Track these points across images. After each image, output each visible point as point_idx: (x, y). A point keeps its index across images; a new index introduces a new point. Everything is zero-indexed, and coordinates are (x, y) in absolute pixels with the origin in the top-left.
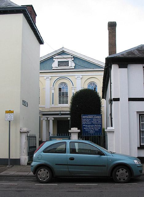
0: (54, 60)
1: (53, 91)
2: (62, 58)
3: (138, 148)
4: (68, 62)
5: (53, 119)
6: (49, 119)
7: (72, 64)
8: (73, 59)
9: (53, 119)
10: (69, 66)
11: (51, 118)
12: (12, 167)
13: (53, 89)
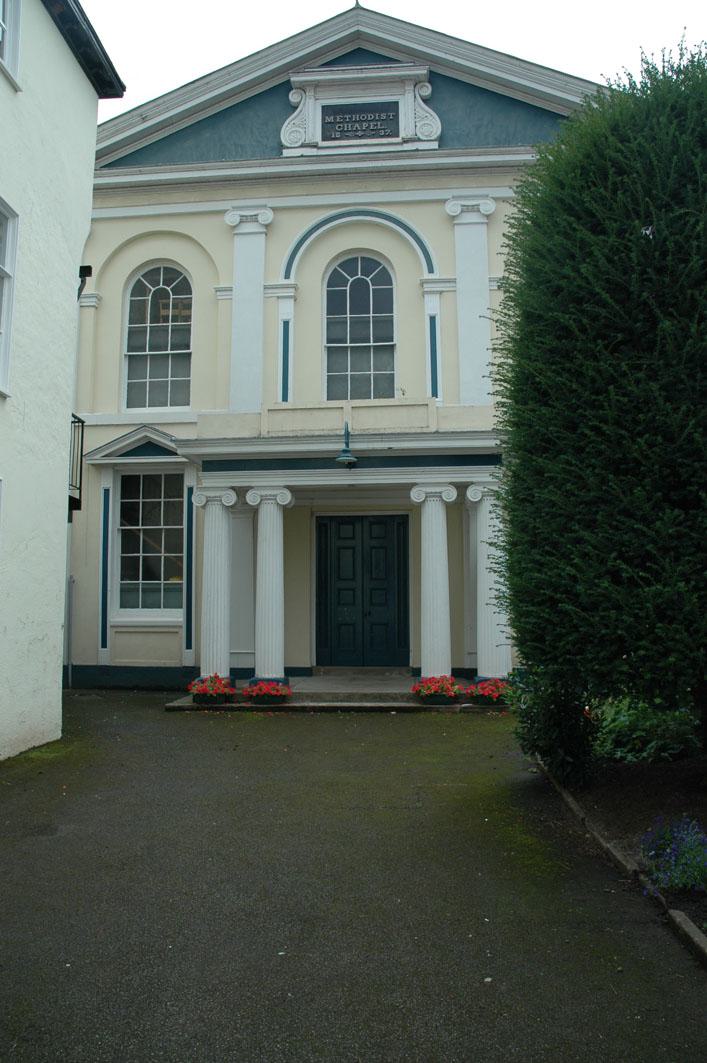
0: (293, 97)
1: (286, 310)
2: (359, 88)
3: (94, 189)
4: (394, 107)
5: (286, 498)
6: (251, 498)
7: (418, 121)
8: (427, 91)
9: (286, 498)
10: (403, 134)
11: (272, 491)
12: (478, 713)
13: (291, 292)
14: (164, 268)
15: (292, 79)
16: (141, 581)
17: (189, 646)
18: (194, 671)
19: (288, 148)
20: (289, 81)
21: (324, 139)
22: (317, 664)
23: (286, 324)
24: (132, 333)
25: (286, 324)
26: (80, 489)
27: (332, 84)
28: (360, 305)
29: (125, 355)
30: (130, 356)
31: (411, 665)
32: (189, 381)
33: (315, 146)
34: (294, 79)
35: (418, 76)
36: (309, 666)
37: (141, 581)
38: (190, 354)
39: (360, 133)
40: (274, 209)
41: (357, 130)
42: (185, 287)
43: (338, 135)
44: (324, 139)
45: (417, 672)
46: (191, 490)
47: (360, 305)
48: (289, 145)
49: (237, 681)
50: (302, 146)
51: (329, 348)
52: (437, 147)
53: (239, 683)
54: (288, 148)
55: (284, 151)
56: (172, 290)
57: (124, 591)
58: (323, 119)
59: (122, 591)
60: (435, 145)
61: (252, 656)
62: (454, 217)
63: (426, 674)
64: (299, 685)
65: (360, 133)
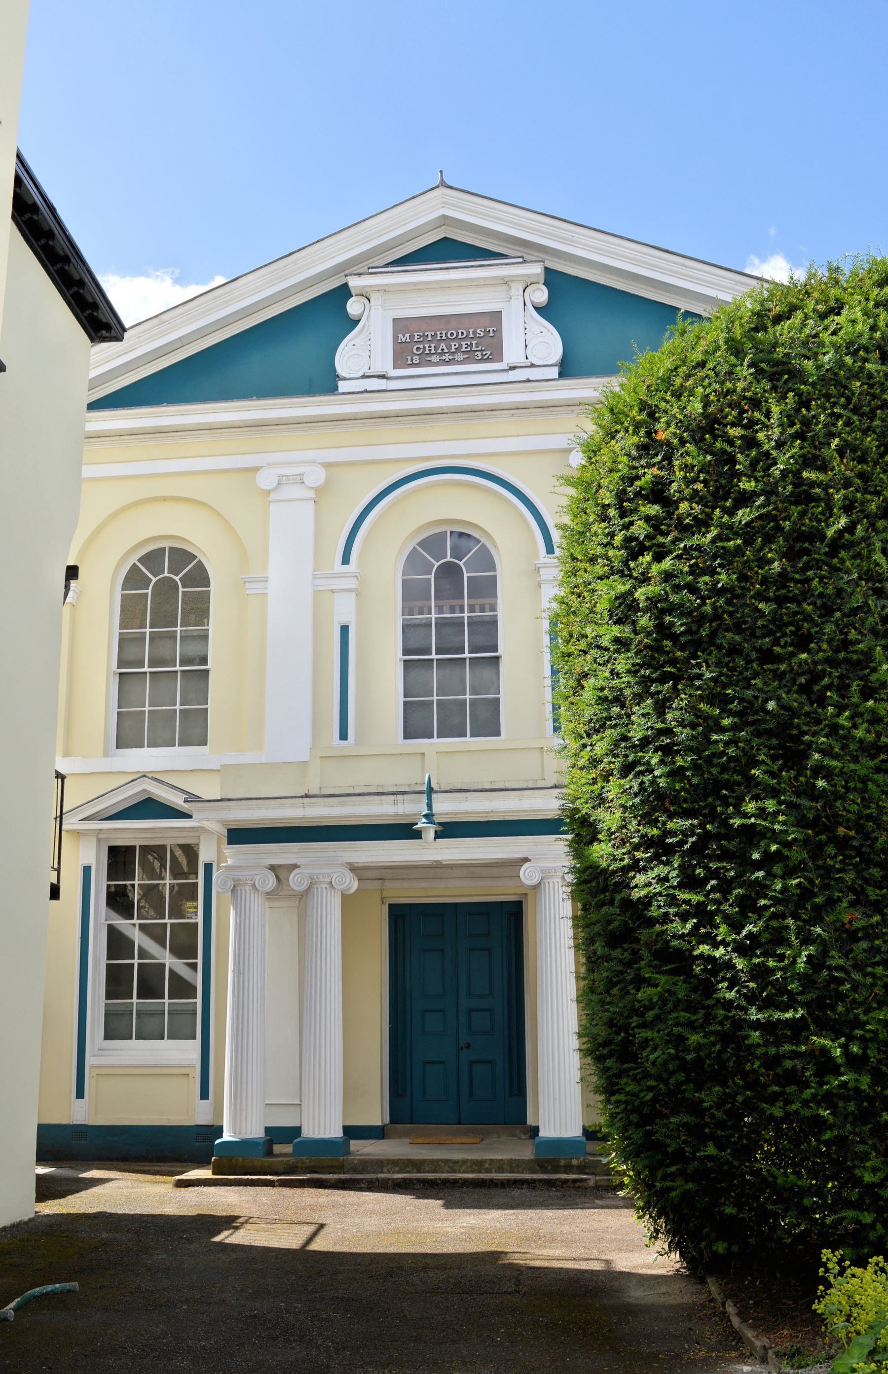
0: (353, 307)
8: (541, 295)
14: (170, 548)
15: (351, 284)
16: (135, 1000)
17: (204, 1095)
18: (297, 1131)
19: (345, 379)
20: (346, 285)
21: (395, 367)
22: (392, 1121)
23: (345, 629)
24: (123, 641)
25: (345, 629)
26: (58, 870)
27: (401, 289)
28: (164, 617)
29: (115, 673)
30: (120, 674)
31: (528, 1123)
32: (206, 710)
33: (383, 377)
34: (354, 283)
35: (528, 276)
36: (379, 1123)
37: (135, 1000)
38: (207, 671)
39: (447, 357)
40: (328, 465)
41: (443, 353)
42: (200, 577)
43: (416, 360)
44: (395, 367)
45: (535, 1130)
46: (208, 867)
47: (164, 617)
48: (348, 376)
49: (352, 1142)
50: (364, 377)
51: (405, 661)
52: (557, 376)
53: (277, 1148)
54: (345, 379)
55: (341, 384)
56: (180, 579)
57: (109, 1015)
58: (395, 337)
59: (107, 1015)
60: (554, 372)
61: (298, 1108)
62: (268, 492)
63: (545, 1133)
64: (362, 1148)
65: (447, 357)
